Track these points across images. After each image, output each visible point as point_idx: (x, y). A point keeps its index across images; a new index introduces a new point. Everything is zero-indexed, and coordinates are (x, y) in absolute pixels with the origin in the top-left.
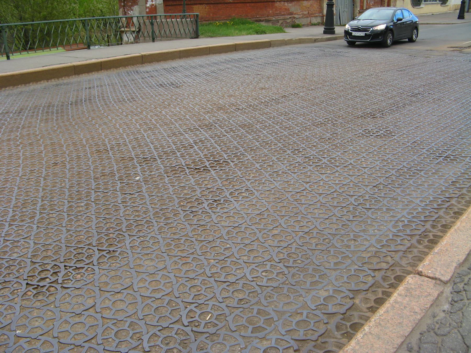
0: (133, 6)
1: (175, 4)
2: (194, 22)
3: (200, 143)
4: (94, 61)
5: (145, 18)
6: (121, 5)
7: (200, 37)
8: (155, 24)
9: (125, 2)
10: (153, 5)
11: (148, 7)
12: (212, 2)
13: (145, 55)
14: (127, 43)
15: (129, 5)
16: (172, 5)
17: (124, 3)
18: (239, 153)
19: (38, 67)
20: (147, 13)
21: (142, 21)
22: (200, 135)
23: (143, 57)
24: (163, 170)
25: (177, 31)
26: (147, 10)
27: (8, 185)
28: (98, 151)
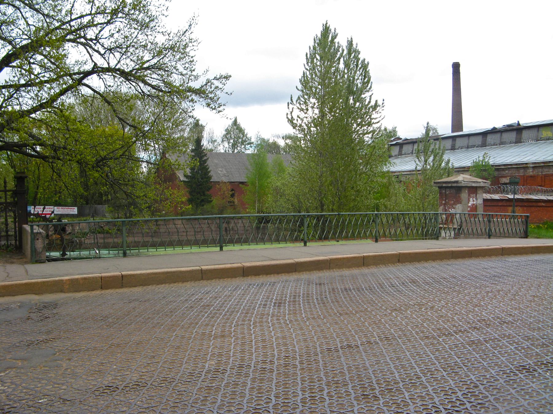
0: (456, 205)
1: (493, 205)
2: (525, 223)
3: (402, 370)
4: (465, 249)
5: (467, 216)
6: (442, 203)
7: (529, 237)
8: (492, 222)
9: (447, 201)
10: (474, 204)
11: (470, 206)
12: (526, 205)
13: (505, 248)
14: (444, 238)
15: (450, 203)
16: (490, 206)
17: (445, 201)
18: (448, 387)
19: (172, 268)
20: (469, 211)
21: (463, 219)
22: (424, 355)
23: (503, 249)
24: (378, 391)
25: (506, 230)
26: (469, 209)
27: (214, 384)
28: (263, 369)
